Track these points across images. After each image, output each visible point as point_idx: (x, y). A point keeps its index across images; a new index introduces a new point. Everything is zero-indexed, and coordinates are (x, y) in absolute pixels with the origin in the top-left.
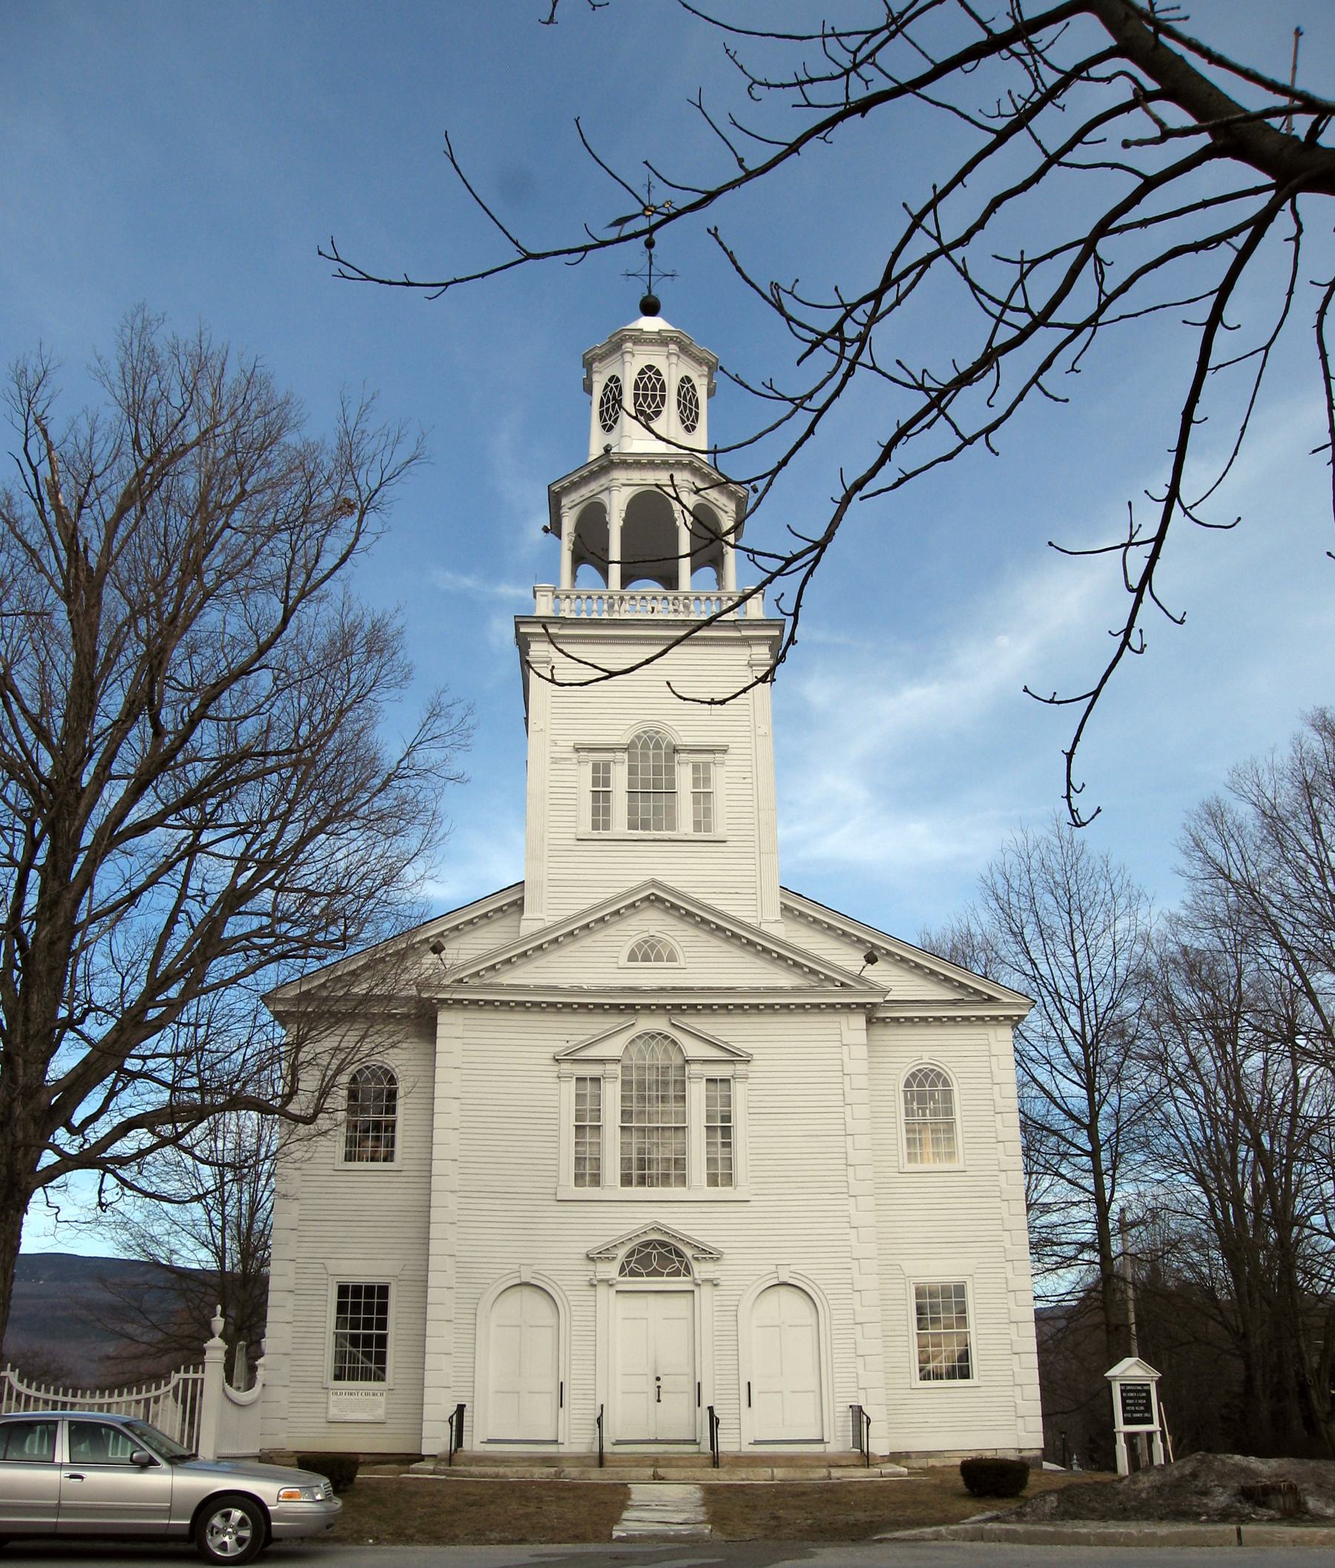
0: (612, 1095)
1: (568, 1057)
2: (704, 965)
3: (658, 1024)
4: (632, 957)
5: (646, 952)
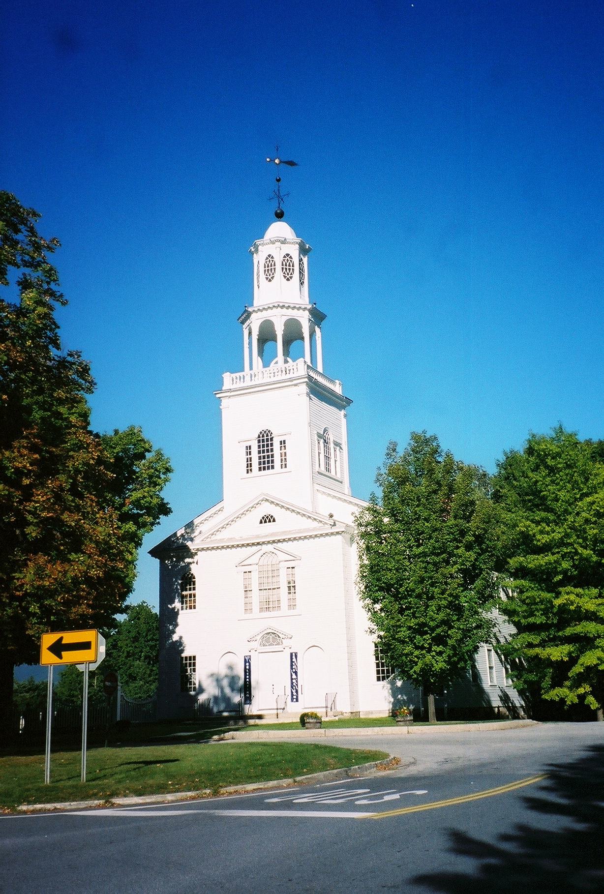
0: (255, 576)
1: (241, 564)
2: (286, 523)
3: (270, 548)
4: (261, 522)
5: (268, 519)
